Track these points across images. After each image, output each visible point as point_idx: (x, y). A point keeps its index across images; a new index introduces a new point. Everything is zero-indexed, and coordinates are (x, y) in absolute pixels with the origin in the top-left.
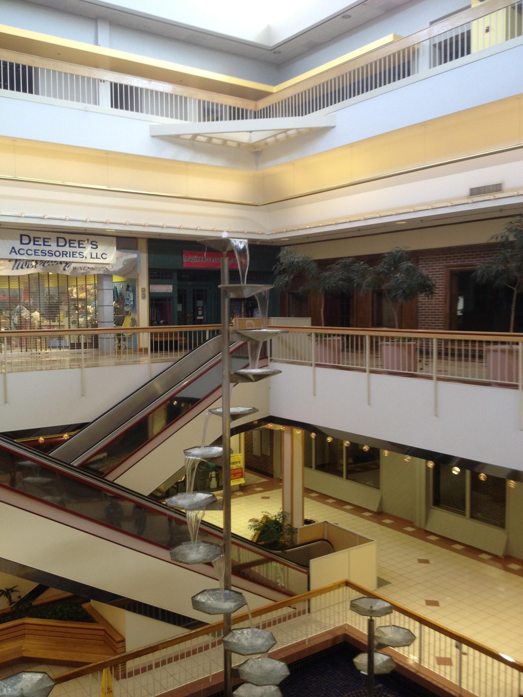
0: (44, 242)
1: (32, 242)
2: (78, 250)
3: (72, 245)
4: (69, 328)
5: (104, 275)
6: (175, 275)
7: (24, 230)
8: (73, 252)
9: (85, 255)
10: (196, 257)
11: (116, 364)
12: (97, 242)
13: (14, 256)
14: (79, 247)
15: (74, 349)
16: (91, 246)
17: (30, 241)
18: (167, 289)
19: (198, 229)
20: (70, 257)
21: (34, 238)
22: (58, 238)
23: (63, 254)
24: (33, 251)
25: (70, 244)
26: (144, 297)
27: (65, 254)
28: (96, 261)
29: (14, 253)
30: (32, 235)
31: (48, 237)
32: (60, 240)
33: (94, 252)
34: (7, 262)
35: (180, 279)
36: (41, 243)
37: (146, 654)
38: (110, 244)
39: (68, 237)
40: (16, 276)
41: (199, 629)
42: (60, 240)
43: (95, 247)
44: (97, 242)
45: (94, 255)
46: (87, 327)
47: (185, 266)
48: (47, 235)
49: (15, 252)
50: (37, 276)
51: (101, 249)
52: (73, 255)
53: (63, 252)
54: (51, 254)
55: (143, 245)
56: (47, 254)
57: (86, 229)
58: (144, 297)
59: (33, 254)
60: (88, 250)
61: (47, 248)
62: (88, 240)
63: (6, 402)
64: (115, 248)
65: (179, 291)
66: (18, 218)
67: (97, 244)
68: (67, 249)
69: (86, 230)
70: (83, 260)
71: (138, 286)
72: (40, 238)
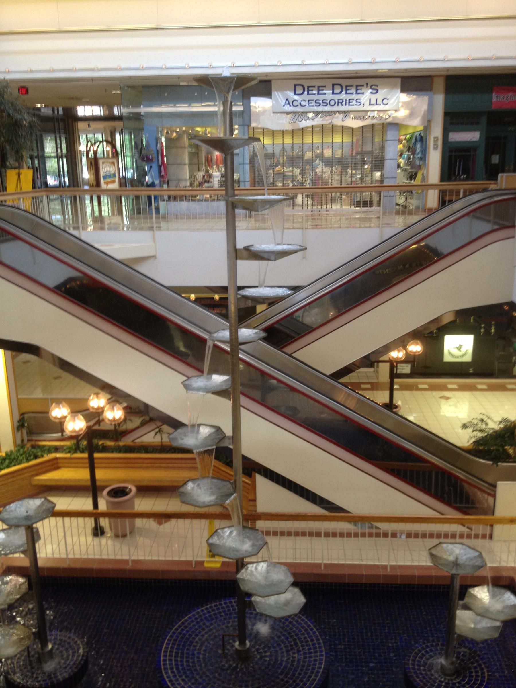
0: (319, 90)
1: (306, 93)
2: (355, 96)
3: (310, 92)
4: (341, 185)
5: (390, 124)
6: (484, 120)
7: (297, 79)
8: (349, 100)
9: (362, 102)
10: (510, 94)
11: (256, 229)
12: (377, 86)
13: (288, 108)
14: (357, 93)
15: (367, 206)
16: (370, 91)
17: (304, 91)
18: (472, 136)
19: (494, 57)
20: (346, 105)
21: (308, 87)
22: (333, 85)
23: (338, 103)
24: (307, 102)
25: (346, 90)
26: (436, 148)
27: (340, 102)
28: (375, 108)
29: (288, 106)
30: (306, 84)
31: (361, 84)
32: (335, 86)
33: (373, 98)
34: (284, 115)
35: (490, 123)
36: (315, 92)
37: (300, 520)
38: (393, 87)
39: (344, 82)
40: (281, 131)
41: (337, 514)
42: (335, 86)
43: (375, 91)
44: (377, 86)
45: (373, 102)
46: (254, 186)
47: (494, 107)
48: (317, 83)
49: (289, 104)
50: (381, 126)
51: (383, 92)
52: (349, 102)
53: (338, 100)
54: (326, 103)
55: (440, 84)
56: (322, 104)
57: (356, 72)
58: (436, 148)
59: (307, 105)
60: (367, 95)
61: (321, 97)
62: (367, 84)
63: (155, 256)
64: (399, 90)
65: (488, 138)
66: (300, 67)
67: (378, 88)
68: (343, 96)
69: (356, 73)
70: (361, 108)
71: (430, 134)
72: (314, 87)
